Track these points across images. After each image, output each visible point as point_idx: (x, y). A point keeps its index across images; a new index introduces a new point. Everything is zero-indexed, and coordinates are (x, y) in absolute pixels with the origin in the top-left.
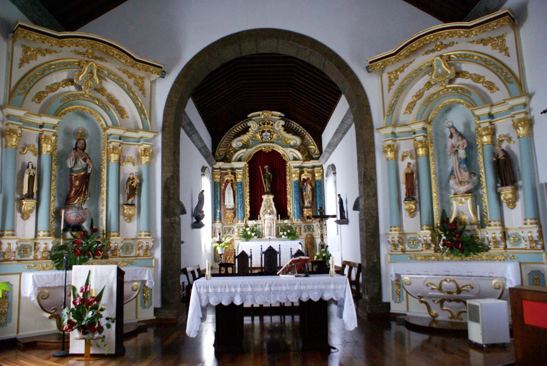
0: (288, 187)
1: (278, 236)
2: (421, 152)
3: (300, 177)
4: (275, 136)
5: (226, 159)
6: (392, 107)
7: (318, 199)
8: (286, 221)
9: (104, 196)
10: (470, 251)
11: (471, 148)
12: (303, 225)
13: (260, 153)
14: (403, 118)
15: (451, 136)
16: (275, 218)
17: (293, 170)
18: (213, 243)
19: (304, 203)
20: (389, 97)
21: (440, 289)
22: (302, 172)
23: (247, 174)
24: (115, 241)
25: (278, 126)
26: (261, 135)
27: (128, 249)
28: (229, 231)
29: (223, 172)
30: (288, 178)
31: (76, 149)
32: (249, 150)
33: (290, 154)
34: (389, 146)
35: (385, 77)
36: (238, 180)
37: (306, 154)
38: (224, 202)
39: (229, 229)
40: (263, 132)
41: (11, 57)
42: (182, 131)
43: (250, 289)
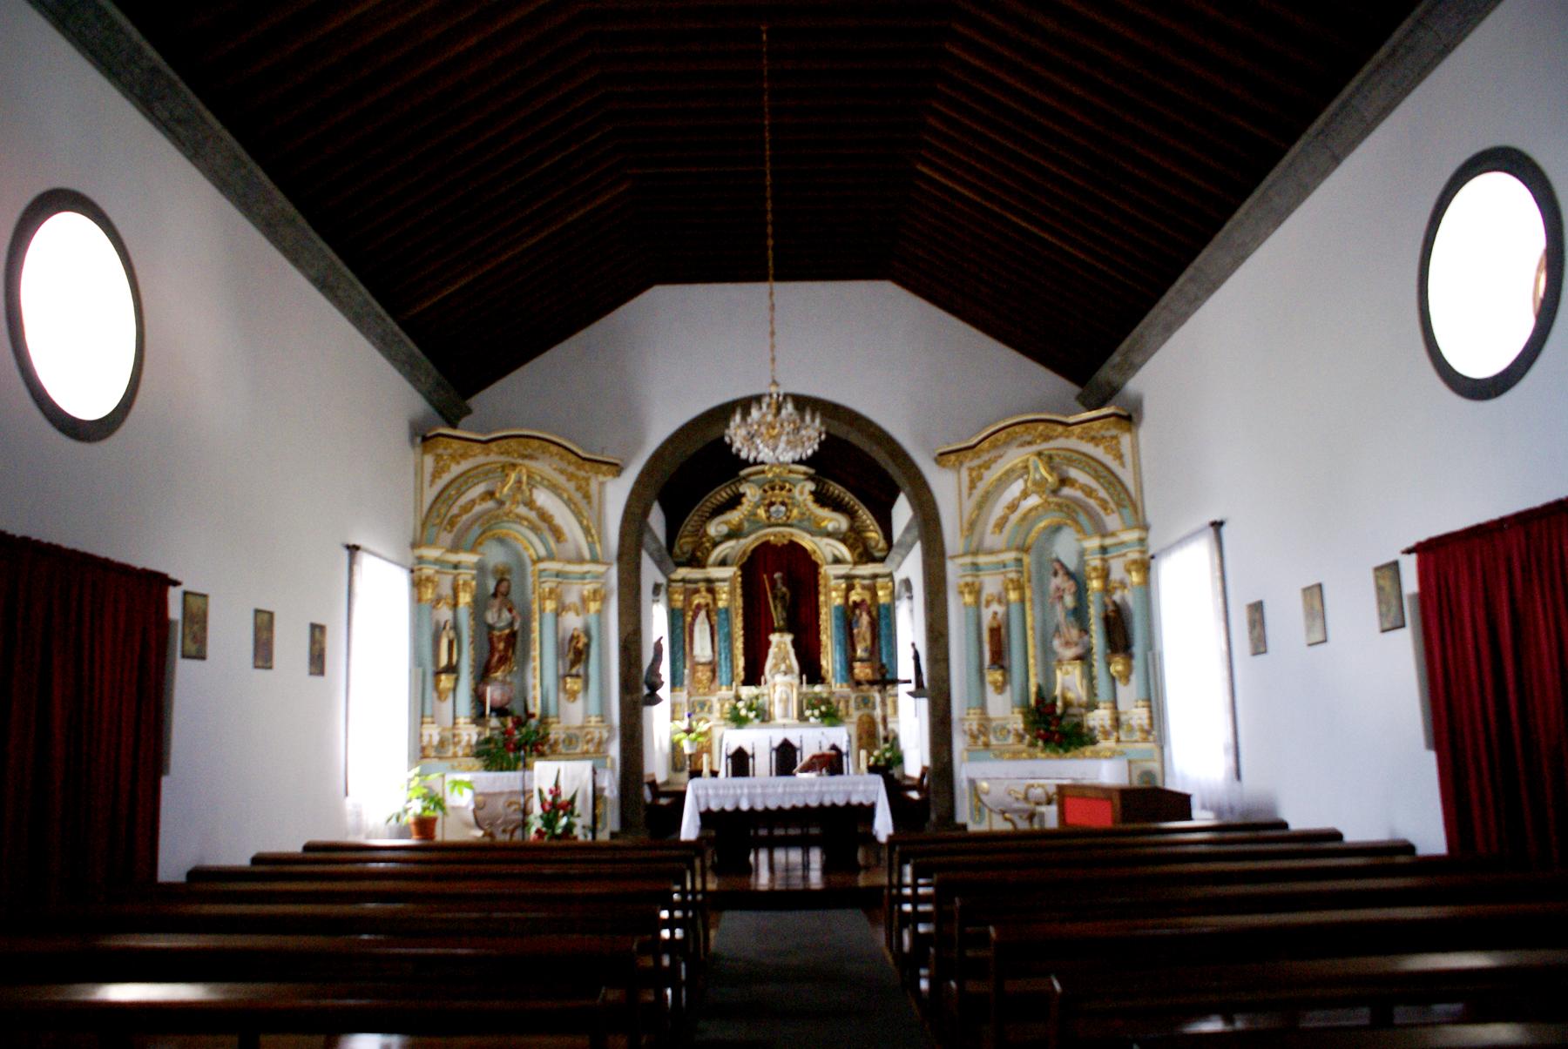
0: (823, 617)
1: (802, 717)
2: (1013, 596)
3: (847, 598)
4: (795, 512)
5: (696, 561)
6: (972, 525)
7: (883, 643)
8: (818, 688)
9: (537, 663)
10: (1070, 744)
11: (1081, 592)
12: (853, 696)
13: (765, 548)
14: (991, 539)
15: (1056, 574)
16: (797, 681)
17: (833, 583)
18: (673, 733)
19: (854, 650)
20: (969, 505)
21: (1026, 798)
22: (850, 588)
23: (739, 591)
24: (556, 732)
25: (802, 493)
26: (767, 511)
27: (570, 742)
28: (702, 709)
29: (690, 588)
30: (822, 598)
31: (495, 595)
32: (743, 541)
33: (824, 549)
34: (967, 585)
35: (965, 473)
36: (721, 604)
37: (860, 550)
38: (692, 649)
39: (703, 705)
40: (772, 504)
41: (419, 470)
42: (645, 555)
43: (759, 790)
